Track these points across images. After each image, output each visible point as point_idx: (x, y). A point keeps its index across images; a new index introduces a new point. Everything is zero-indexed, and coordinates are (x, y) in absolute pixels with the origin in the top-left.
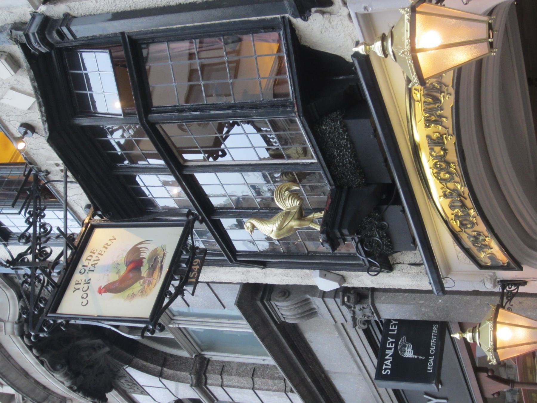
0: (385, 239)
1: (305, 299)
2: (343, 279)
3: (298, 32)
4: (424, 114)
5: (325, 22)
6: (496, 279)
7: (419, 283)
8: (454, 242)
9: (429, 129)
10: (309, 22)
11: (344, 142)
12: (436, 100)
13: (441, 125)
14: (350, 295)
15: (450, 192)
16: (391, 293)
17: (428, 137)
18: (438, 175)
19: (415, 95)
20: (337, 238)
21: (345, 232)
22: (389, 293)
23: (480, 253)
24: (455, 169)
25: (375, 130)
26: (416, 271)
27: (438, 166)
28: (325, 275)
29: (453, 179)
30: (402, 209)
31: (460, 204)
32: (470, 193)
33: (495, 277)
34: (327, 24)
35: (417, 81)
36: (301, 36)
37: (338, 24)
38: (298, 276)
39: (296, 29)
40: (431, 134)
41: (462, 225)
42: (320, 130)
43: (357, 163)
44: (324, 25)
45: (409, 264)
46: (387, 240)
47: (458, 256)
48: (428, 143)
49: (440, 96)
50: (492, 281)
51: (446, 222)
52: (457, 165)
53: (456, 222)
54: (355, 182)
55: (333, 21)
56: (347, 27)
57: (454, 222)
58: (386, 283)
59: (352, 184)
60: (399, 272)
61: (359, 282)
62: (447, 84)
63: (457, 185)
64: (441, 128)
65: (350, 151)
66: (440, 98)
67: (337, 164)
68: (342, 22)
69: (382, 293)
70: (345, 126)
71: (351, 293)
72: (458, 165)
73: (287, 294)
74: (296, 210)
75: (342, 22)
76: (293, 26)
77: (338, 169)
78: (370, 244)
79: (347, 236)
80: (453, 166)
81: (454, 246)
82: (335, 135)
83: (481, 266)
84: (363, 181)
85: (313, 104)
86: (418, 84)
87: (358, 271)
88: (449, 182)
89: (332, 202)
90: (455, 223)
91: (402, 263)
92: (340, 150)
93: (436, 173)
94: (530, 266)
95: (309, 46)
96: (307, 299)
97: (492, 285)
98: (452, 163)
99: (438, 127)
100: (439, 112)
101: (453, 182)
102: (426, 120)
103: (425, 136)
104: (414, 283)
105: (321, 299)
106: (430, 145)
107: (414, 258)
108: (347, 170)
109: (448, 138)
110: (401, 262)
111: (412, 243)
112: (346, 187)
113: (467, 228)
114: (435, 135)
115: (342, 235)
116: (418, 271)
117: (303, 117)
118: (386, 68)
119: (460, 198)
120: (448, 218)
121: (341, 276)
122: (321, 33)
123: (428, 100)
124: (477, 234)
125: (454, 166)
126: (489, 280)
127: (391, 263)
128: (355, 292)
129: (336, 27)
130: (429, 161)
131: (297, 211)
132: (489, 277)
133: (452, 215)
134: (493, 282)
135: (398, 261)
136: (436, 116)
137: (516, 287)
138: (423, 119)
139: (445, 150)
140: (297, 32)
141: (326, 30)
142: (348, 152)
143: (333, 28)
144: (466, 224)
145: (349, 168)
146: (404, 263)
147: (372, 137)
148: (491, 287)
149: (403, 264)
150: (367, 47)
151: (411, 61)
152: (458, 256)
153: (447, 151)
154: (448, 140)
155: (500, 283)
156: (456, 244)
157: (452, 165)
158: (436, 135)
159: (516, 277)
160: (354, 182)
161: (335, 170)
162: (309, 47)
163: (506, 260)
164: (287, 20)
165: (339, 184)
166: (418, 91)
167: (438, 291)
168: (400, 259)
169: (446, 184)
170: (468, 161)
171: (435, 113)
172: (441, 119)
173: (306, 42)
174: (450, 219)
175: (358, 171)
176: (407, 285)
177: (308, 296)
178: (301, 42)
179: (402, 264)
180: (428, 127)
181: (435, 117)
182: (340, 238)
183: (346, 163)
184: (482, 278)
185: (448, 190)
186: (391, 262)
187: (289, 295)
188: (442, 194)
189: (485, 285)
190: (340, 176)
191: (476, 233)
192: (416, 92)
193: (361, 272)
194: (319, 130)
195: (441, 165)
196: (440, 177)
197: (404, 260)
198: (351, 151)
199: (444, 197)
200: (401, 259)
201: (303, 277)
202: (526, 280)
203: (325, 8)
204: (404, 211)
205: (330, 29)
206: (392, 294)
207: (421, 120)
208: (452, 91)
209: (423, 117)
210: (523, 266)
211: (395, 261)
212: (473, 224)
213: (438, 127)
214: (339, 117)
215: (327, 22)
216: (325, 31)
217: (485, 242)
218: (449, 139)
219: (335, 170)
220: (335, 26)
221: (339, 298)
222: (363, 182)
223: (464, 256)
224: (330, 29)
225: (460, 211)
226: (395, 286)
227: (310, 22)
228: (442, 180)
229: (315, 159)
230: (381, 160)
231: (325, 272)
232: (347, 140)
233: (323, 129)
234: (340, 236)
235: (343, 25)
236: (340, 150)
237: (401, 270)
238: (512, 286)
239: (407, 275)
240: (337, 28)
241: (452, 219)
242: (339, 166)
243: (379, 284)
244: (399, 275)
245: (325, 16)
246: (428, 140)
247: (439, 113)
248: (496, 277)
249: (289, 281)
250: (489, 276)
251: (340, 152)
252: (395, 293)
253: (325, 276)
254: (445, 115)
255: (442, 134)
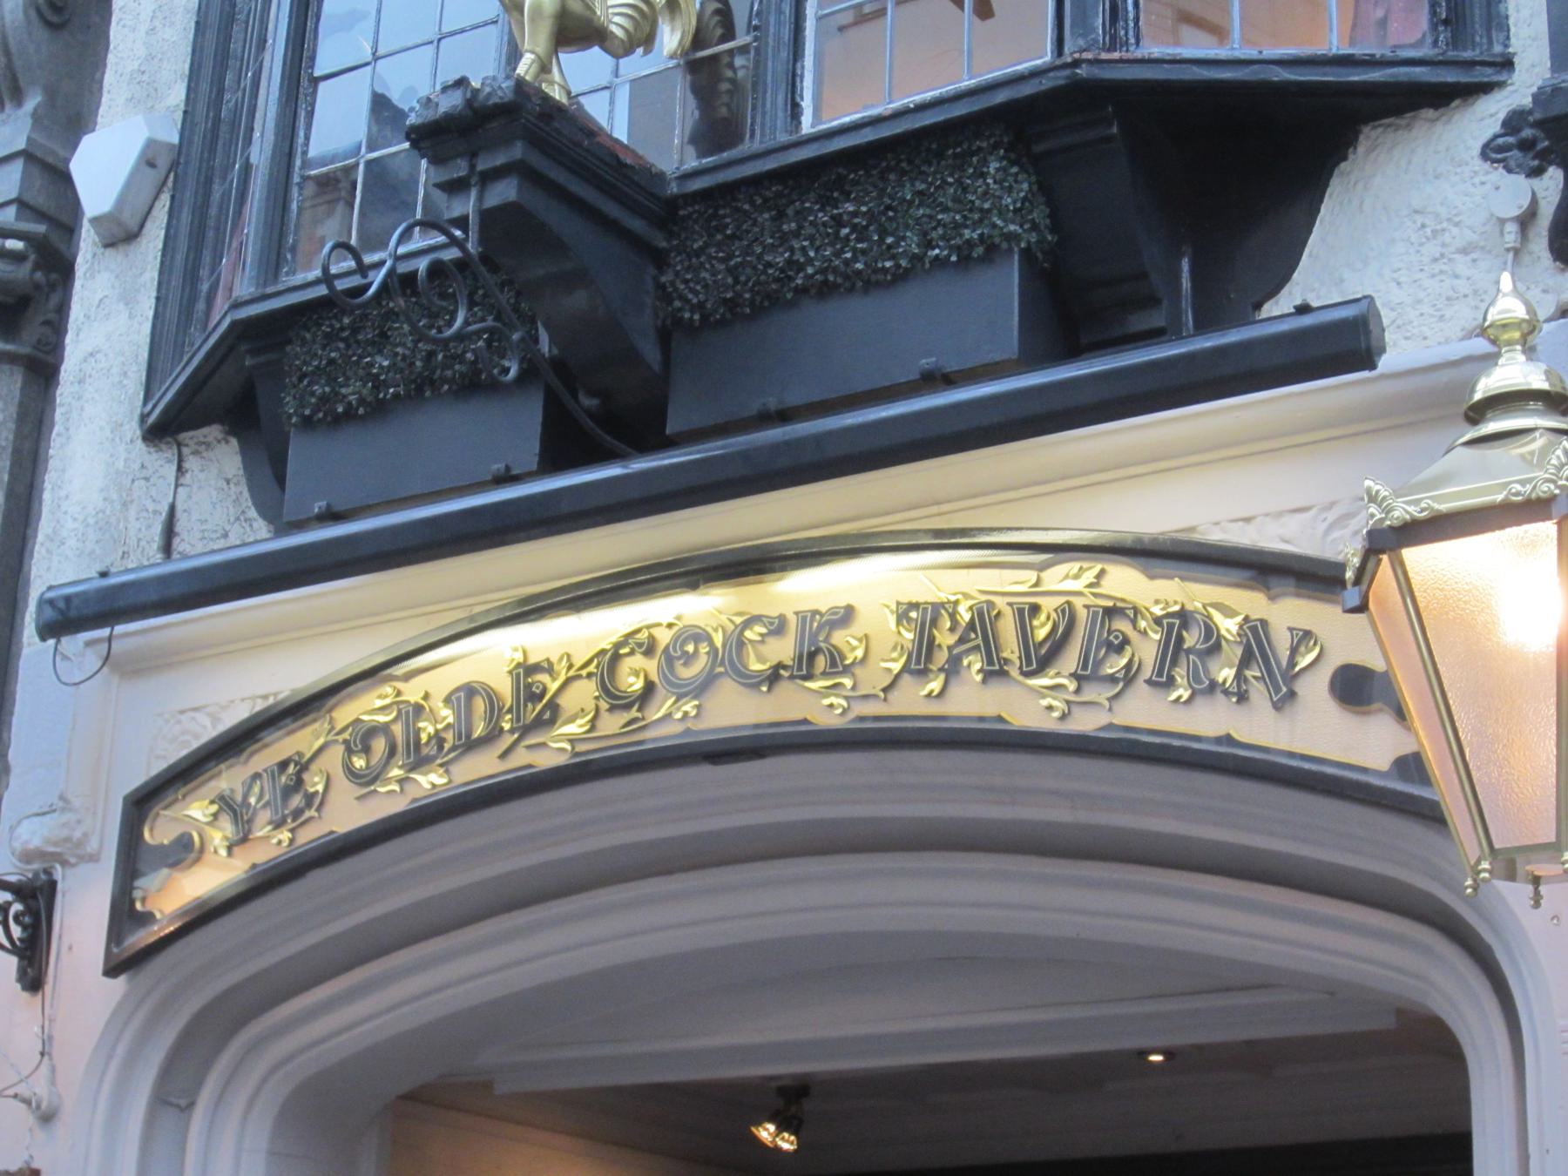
0: (365, 392)
1: (22, 84)
2: (121, 235)
3: (1428, 120)
4: (971, 602)
5: (1470, 228)
6: (65, 863)
7: (72, 542)
8: (271, 701)
9: (892, 620)
10: (1479, 165)
11: (912, 243)
12: (1041, 658)
13: (905, 669)
14: (28, 266)
15: (545, 690)
16: (11, 437)
17: (846, 616)
18: (640, 645)
19: (1075, 570)
20: (473, 155)
21: (504, 192)
22: (12, 426)
23: (212, 802)
24: (668, 716)
25: (948, 380)
26: (132, 533)
27: (690, 648)
28: (151, 164)
29: (612, 709)
30: (515, 472)
31: (479, 730)
32: (532, 775)
33: (73, 860)
34: (1457, 237)
35: (1396, 514)
36: (1409, 127)
37: (1456, 282)
38: (150, 57)
39: (1441, 110)
40: (858, 628)
41: (363, 737)
42: (980, 149)
43: (789, 296)
44: (1457, 224)
45: (172, 509)
46: (361, 401)
47: (196, 709)
48: (815, 612)
49: (1058, 674)
50: (56, 844)
51: (372, 674)
52: (689, 724)
53: (383, 709)
54: (686, 282)
55: (1474, 261)
56: (1442, 316)
57: (387, 701)
58: (82, 409)
59: (679, 268)
60: (137, 466)
61: (96, 302)
62: (1116, 706)
63: (580, 722)
64: (889, 670)
65: (859, 266)
66: (1052, 672)
67: (790, 212)
68: (1466, 296)
69: (16, 400)
70: (993, 251)
71: (34, 270)
72: (688, 732)
73: (55, 19)
74: (599, 13)
75: (1466, 296)
76: (1457, 102)
77: (766, 216)
78: (342, 329)
79: (480, 199)
80: (687, 708)
81: (253, 698)
82: (946, 210)
83: (143, 803)
84: (692, 312)
85: (1115, 130)
86: (1382, 520)
87: (158, 299)
88: (603, 687)
89: (621, 165)
90: (379, 703)
91: (182, 481)
92: (866, 228)
93: (652, 639)
94: (120, 1005)
95: (1351, 157)
96: (18, 95)
97: (36, 843)
98: (698, 707)
99: (895, 655)
100: (978, 666)
101: (597, 710)
102: (937, 607)
103: (850, 602)
104: (70, 525)
105: (21, 144)
106: (804, 619)
107: (203, 531)
108: (759, 250)
109: (837, 696)
110: (188, 476)
111: (329, 506)
112: (664, 244)
113: (349, 751)
114: (854, 643)
115: (489, 178)
116: (133, 542)
117: (1068, 77)
118: (1223, 459)
119: (512, 731)
120: (408, 677)
121: (136, 229)
122: (1416, 212)
123: (1043, 625)
124: (317, 792)
125: (686, 714)
126: (65, 833)
127: (184, 436)
128: (37, 287)
129: (1441, 272)
130: (720, 613)
131: (595, 13)
132: (78, 834)
133: (422, 694)
134: (52, 849)
135: (191, 463)
136: (955, 652)
137: (18, 943)
138: (942, 597)
139: (774, 676)
140: (1429, 113)
141: (1428, 231)
142: (855, 259)
143: (1435, 260)
144: (366, 750)
145: (768, 258)
146: (180, 489)
147: (926, 362)
148: (25, 837)
149: (177, 486)
150: (1517, 335)
151: (1518, 494)
152: (196, 709)
153: (764, 689)
154: (827, 696)
155: (43, 877)
156: (260, 706)
157: (689, 707)
158: (854, 649)
159: (64, 948)
160: (689, 276)
161: (759, 201)
162: (1345, 158)
163: (161, 912)
164: (1495, 78)
165: (681, 213)
166: (1091, 585)
167: (62, 605)
168: (202, 471)
169: (590, 675)
170: (706, 771)
171: (977, 648)
172: (941, 670)
173: (1369, 151)
174: (400, 685)
175: (747, 296)
176: (63, 493)
177: (32, 102)
178: (1374, 128)
179: (177, 479)
180: (902, 617)
181: (950, 648)
182: (472, 167)
183: (792, 250)
184: (76, 802)
185: (553, 687)
186: (191, 433)
187: (49, 25)
188: (532, 660)
189: (38, 815)
190: (728, 220)
191: (320, 788)
192: (1089, 576)
193: (151, 313)
194: (984, 145)
195: (689, 659)
196: (632, 653)
197: (195, 489)
198: (859, 272)
199: (519, 665)
200: (202, 476)
201: (145, 78)
202: (48, 988)
203: (1545, 233)
204: (506, 478)
205: (1432, 249)
206: (7, 439)
207: (939, 590)
208: (1086, 723)
209: (953, 598)
210: (122, 979)
211: (196, 453)
212: (367, 779)
213: (895, 655)
214: (1033, 237)
215: (1469, 236)
216: (1423, 226)
217: (270, 823)
218: (826, 702)
219: (759, 201)
220: (1444, 268)
221: (18, 218)
222: (687, 315)
223: (196, 736)
224: (1432, 249)
225: (440, 726)
226: (62, 446)
227: (1477, 168)
228: (611, 659)
229: (812, 126)
230: (795, 398)
231: (164, 162)
232: (917, 259)
233: (985, 162)
234: (482, 166)
235: (1448, 299)
236: (866, 228)
237: (145, 473)
238: (25, 927)
239: (115, 496)
240: (1433, 276)
241: (399, 693)
242: (780, 216)
243: (79, 383)
244: (120, 464)
245: (1512, 229)
246: (833, 610)
247: (975, 663)
248: (73, 865)
249: (129, 23)
250: (85, 835)
251: (854, 228)
252: (10, 450)
253: (148, 160)
254: (955, 690)
255: (858, 671)
